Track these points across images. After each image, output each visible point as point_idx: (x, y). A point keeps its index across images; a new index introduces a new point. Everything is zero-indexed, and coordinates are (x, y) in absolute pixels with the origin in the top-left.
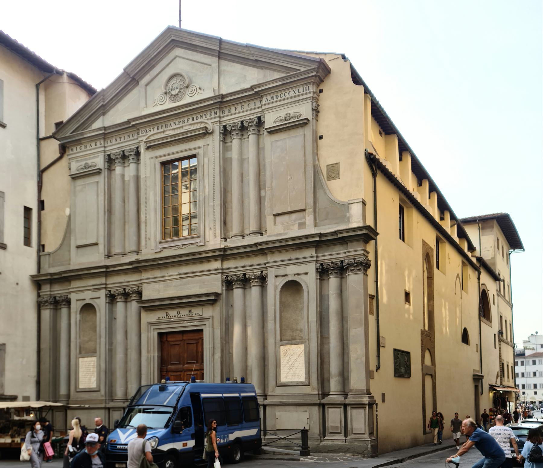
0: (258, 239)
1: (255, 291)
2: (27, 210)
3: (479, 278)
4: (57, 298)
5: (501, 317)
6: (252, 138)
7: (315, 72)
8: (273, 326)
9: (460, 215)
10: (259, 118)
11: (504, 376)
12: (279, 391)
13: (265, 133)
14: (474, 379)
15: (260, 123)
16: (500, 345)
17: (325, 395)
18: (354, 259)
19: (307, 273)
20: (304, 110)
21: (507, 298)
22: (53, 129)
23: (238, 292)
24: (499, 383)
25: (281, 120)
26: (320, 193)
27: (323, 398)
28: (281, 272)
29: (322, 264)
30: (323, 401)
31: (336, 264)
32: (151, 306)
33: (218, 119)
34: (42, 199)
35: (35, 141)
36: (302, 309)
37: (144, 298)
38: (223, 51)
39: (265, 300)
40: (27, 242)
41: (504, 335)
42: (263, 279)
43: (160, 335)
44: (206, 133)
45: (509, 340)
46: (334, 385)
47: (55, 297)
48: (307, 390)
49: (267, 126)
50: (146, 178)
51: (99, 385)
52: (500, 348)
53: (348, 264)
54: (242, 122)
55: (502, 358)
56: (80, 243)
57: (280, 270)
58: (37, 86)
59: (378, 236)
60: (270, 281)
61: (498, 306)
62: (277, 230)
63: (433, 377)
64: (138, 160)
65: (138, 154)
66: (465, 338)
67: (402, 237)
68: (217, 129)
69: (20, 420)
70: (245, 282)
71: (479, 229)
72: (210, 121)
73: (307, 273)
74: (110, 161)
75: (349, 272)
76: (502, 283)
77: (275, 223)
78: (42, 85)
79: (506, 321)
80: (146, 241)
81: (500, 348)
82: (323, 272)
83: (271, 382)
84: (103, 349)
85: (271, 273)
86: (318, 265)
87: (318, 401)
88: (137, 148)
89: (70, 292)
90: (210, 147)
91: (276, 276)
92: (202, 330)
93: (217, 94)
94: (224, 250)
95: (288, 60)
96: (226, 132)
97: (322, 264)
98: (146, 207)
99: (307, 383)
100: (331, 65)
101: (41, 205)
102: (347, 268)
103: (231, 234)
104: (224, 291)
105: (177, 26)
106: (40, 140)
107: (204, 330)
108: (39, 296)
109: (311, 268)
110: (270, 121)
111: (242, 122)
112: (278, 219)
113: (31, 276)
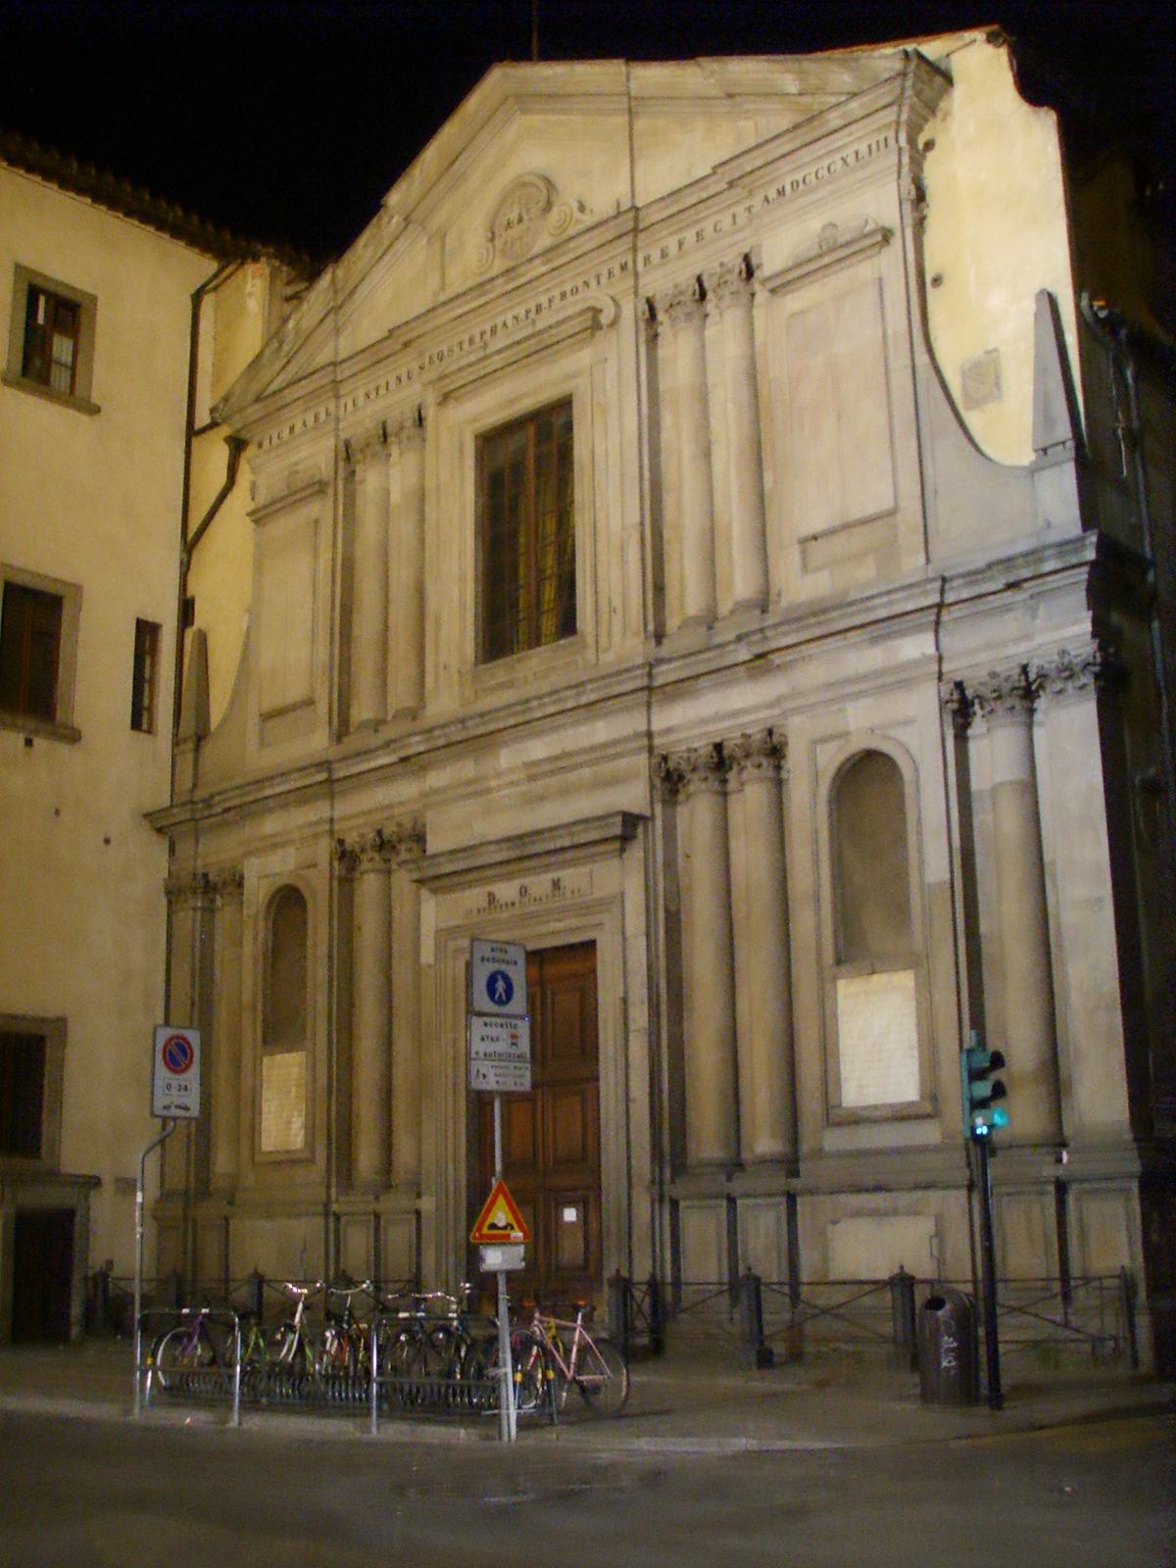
1: (751, 797)
2: (146, 632)
4: (212, 877)
8: (813, 924)
9: (167, 803)
23: (697, 813)
29: (959, 685)
31: (1007, 679)
34: (189, 594)
37: (428, 853)
39: (785, 796)
40: (140, 717)
42: (775, 752)
44: (594, 324)
48: (929, 1133)
50: (438, 487)
51: (310, 1144)
64: (424, 447)
67: (136, 725)
68: (630, 311)
83: (810, 1105)
84: (320, 1028)
90: (611, 368)
92: (590, 946)
95: (800, 855)
99: (928, 1108)
101: (187, 610)
102: (1041, 687)
104: (658, 809)
106: (192, 432)
107: (598, 941)
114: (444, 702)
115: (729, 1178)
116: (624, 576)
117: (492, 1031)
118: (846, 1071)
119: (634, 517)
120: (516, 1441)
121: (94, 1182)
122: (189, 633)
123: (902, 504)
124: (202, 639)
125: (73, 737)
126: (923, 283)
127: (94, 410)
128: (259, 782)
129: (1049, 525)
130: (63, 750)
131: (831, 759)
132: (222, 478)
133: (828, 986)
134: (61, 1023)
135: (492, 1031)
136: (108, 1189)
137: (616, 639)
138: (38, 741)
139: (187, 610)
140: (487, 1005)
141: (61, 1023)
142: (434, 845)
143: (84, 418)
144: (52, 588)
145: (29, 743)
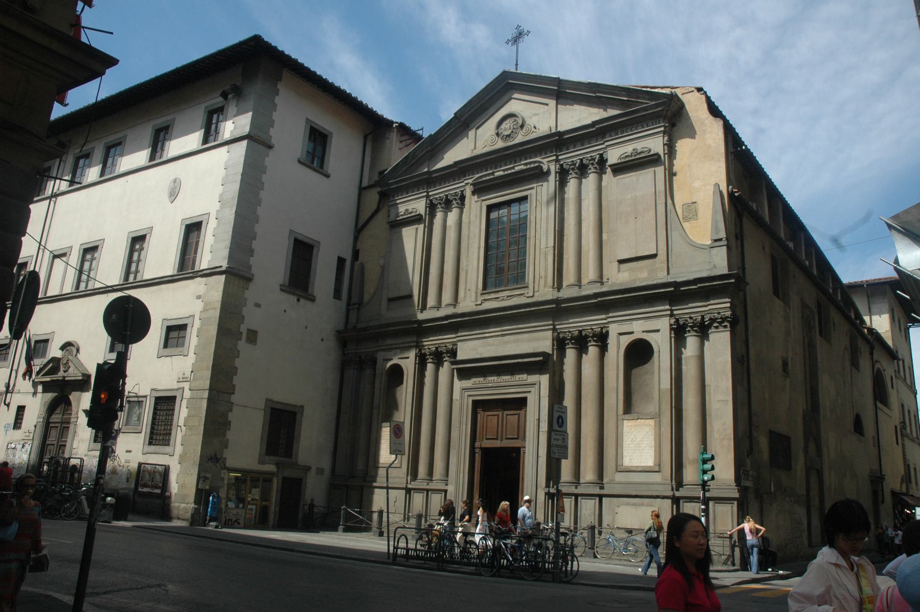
0: (597, 289)
2: (341, 261)
3: (872, 354)
5: (902, 405)
6: (590, 181)
7: (668, 112)
10: (601, 155)
11: (910, 482)
12: (619, 477)
13: (609, 170)
14: (872, 481)
15: (602, 161)
16: (902, 440)
17: (679, 484)
18: (719, 313)
19: (658, 331)
20: (655, 144)
21: (908, 382)
22: (376, 178)
24: (904, 490)
25: (626, 157)
26: (675, 236)
27: (677, 490)
28: (625, 328)
30: (677, 494)
32: (467, 371)
33: (554, 158)
35: (356, 192)
36: (653, 373)
38: (562, 92)
41: (908, 428)
43: (474, 402)
45: (915, 435)
46: (690, 474)
47: (360, 357)
48: (657, 478)
49: (610, 162)
52: (903, 445)
53: (710, 319)
54: (581, 160)
55: (907, 457)
56: (391, 296)
57: (623, 329)
58: (365, 138)
59: (748, 287)
60: (612, 341)
61: (898, 392)
62: (620, 278)
63: (820, 474)
65: (463, 198)
66: (858, 426)
68: (553, 168)
69: (52, 381)
70: (581, 342)
71: (868, 297)
72: (547, 162)
73: (658, 331)
74: (432, 208)
75: (713, 330)
76: (901, 362)
77: (619, 271)
78: (370, 137)
79: (909, 411)
80: (465, 293)
81: (903, 445)
82: (679, 332)
85: (614, 330)
86: (673, 321)
87: (670, 493)
88: (462, 191)
89: (377, 351)
91: (621, 334)
93: (553, 131)
94: (557, 301)
96: (563, 175)
97: (677, 320)
98: (467, 257)
100: (684, 99)
102: (710, 326)
103: (565, 284)
105: (513, 70)
106: (362, 190)
108: (344, 354)
109: (664, 324)
110: (614, 156)
111: (581, 160)
112: (624, 266)
113: (338, 332)
114: (469, 302)
115: (576, 488)
116: (546, 266)
117: (558, 437)
118: (625, 453)
119: (551, 243)
120: (198, 518)
121: (308, 469)
122: (357, 263)
123: (659, 253)
124: (362, 266)
125: (312, 299)
126: (671, 175)
127: (328, 176)
128: (388, 325)
129: (715, 267)
130: (308, 303)
131: (626, 341)
132: (374, 206)
133: (620, 422)
134: (267, 400)
135: (558, 437)
136: (313, 471)
137: (542, 287)
138: (301, 300)
139: (356, 254)
140: (557, 428)
141: (267, 400)
142: (460, 356)
143: (325, 178)
144: (310, 242)
145: (298, 300)
